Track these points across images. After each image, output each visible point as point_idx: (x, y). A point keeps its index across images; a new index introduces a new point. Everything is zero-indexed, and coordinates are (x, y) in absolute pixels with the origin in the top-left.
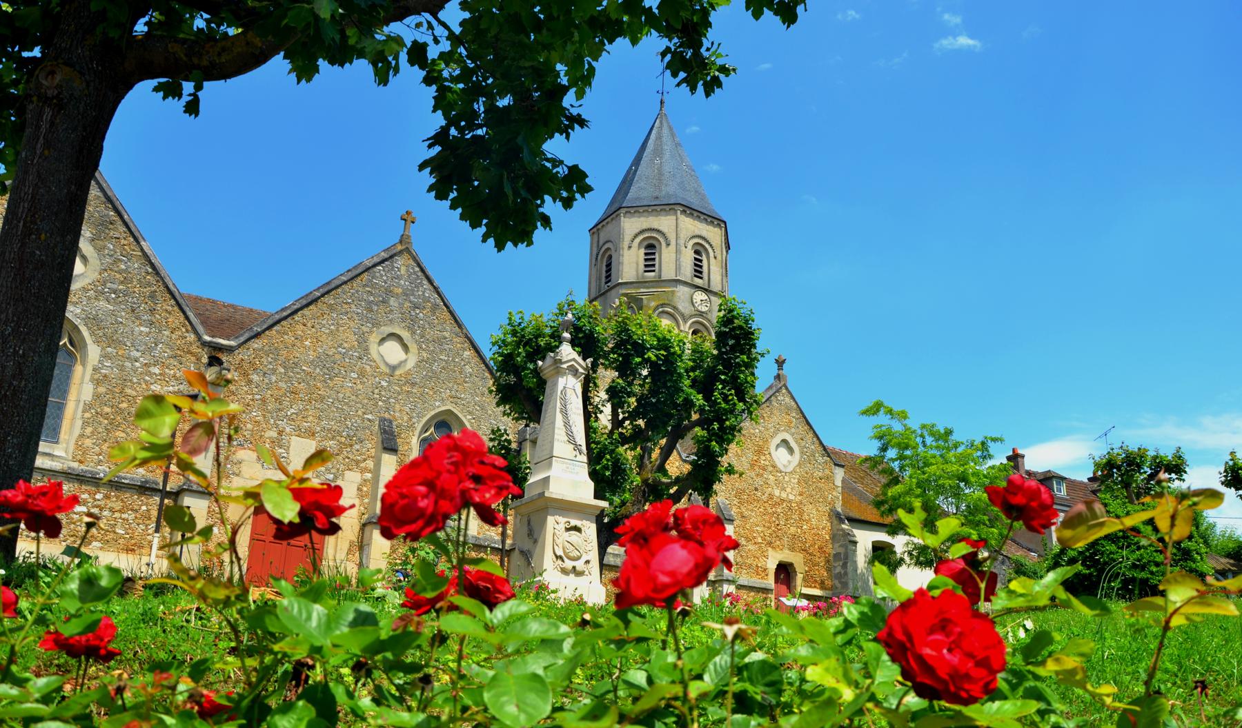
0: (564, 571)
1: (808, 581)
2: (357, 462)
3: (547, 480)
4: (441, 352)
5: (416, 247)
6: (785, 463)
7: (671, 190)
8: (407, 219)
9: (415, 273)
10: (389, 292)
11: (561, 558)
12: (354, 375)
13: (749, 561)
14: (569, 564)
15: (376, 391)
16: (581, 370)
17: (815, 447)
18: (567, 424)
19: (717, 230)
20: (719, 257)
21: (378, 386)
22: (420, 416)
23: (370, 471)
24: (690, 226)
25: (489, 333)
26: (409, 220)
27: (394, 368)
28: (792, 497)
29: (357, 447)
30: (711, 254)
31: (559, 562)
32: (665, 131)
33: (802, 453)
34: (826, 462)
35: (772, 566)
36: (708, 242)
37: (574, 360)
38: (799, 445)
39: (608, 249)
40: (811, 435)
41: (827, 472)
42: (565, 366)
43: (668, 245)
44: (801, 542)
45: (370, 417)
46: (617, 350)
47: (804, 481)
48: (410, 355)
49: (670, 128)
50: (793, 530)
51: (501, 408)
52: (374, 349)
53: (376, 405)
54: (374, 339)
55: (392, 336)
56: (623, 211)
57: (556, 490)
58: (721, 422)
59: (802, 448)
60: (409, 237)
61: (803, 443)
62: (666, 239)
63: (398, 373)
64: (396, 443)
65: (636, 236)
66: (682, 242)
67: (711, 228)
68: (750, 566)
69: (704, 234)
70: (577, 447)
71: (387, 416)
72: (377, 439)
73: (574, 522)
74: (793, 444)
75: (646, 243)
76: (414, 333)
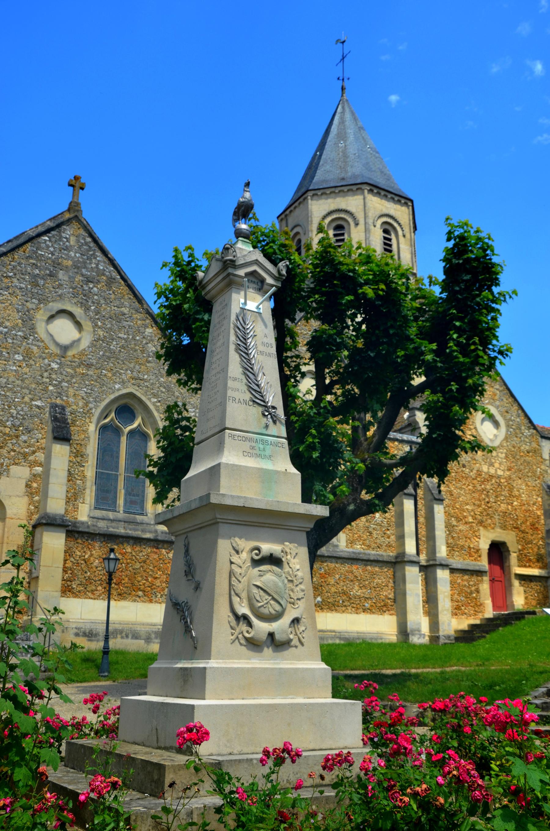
0: (253, 644)
1: (523, 561)
2: (25, 456)
3: (215, 471)
4: (120, 330)
5: (87, 215)
6: (491, 437)
7: (356, 170)
8: (76, 184)
9: (86, 244)
10: (57, 264)
11: (245, 618)
12: (18, 357)
13: (461, 542)
14: (262, 628)
15: (46, 374)
16: (269, 280)
17: (521, 419)
18: (248, 369)
19: (404, 209)
20: (408, 235)
21: (48, 369)
22: (97, 400)
23: (40, 465)
24: (378, 205)
25: (152, 279)
26: (78, 185)
27: (65, 348)
28: (500, 473)
29: (24, 438)
30: (400, 233)
31: (244, 627)
32: (348, 116)
33: (508, 426)
34: (532, 435)
35: (484, 546)
36: (396, 220)
37: (256, 262)
38: (505, 419)
39: (297, 233)
40: (516, 407)
41: (534, 445)
42: (241, 272)
43: (357, 224)
44: (513, 519)
45: (39, 403)
46: (323, 291)
47: (512, 455)
48: (84, 333)
49: (353, 113)
50: (503, 507)
51: (174, 378)
52: (41, 328)
53: (46, 390)
54: (41, 316)
55: (62, 312)
56: (310, 194)
57: (231, 491)
58: (461, 381)
59: (507, 421)
60: (78, 204)
61: (508, 416)
62: (354, 218)
63: (70, 353)
64: (69, 432)
65: (324, 218)
66: (370, 221)
67: (398, 207)
68: (462, 547)
69: (392, 212)
70: (268, 410)
71: (58, 401)
72: (48, 428)
73: (267, 548)
74: (498, 418)
75: (334, 224)
76: (87, 309)
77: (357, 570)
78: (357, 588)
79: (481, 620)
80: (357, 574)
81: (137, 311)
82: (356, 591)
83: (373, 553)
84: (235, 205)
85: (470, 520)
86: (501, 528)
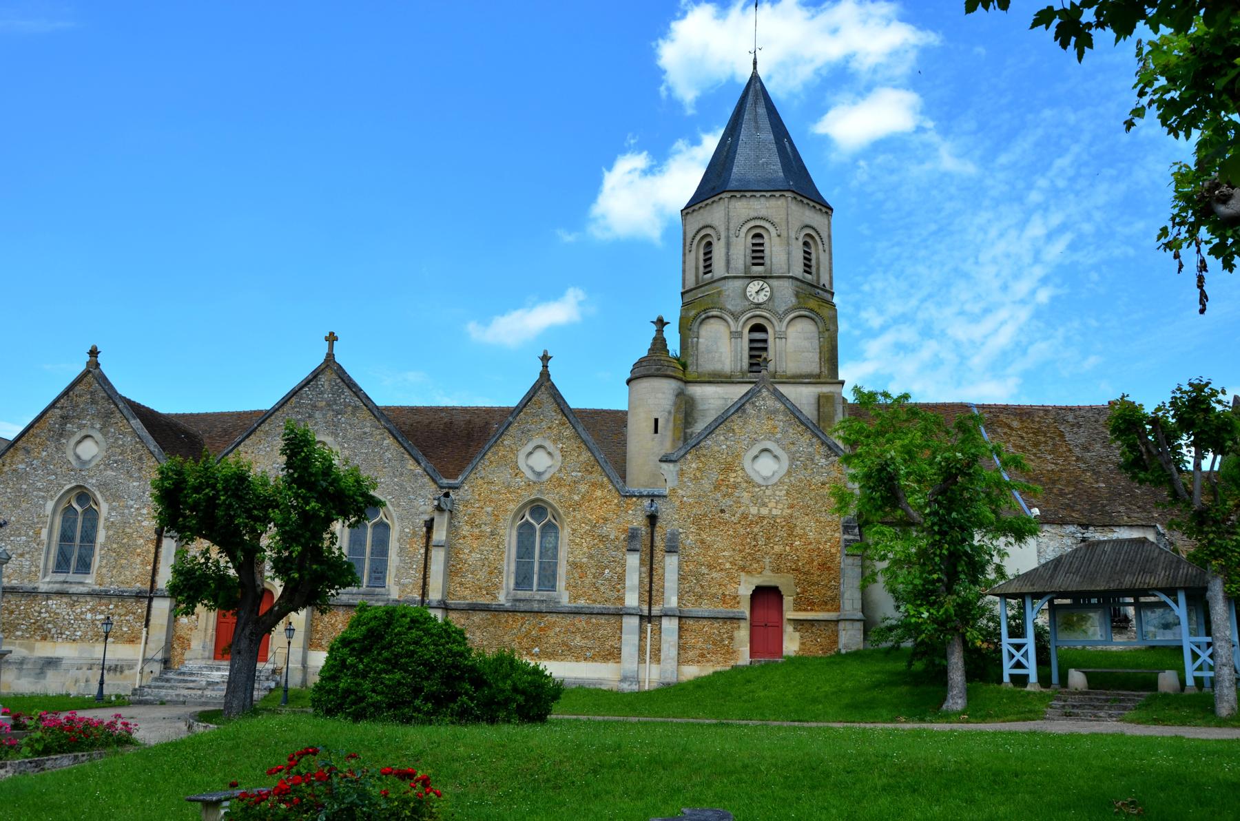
1: (798, 606)
10: (314, 407)
28: (775, 512)
68: (714, 596)
77: (581, 622)
78: (578, 639)
79: (355, 472)
80: (579, 625)
81: (377, 428)
82: (578, 641)
83: (598, 606)
84: (772, 584)
85: (728, 566)
86: (773, 571)
